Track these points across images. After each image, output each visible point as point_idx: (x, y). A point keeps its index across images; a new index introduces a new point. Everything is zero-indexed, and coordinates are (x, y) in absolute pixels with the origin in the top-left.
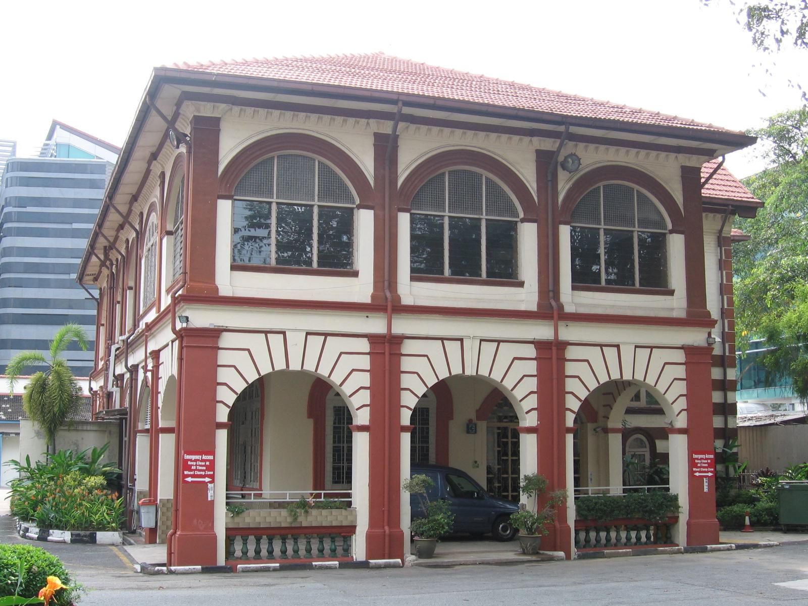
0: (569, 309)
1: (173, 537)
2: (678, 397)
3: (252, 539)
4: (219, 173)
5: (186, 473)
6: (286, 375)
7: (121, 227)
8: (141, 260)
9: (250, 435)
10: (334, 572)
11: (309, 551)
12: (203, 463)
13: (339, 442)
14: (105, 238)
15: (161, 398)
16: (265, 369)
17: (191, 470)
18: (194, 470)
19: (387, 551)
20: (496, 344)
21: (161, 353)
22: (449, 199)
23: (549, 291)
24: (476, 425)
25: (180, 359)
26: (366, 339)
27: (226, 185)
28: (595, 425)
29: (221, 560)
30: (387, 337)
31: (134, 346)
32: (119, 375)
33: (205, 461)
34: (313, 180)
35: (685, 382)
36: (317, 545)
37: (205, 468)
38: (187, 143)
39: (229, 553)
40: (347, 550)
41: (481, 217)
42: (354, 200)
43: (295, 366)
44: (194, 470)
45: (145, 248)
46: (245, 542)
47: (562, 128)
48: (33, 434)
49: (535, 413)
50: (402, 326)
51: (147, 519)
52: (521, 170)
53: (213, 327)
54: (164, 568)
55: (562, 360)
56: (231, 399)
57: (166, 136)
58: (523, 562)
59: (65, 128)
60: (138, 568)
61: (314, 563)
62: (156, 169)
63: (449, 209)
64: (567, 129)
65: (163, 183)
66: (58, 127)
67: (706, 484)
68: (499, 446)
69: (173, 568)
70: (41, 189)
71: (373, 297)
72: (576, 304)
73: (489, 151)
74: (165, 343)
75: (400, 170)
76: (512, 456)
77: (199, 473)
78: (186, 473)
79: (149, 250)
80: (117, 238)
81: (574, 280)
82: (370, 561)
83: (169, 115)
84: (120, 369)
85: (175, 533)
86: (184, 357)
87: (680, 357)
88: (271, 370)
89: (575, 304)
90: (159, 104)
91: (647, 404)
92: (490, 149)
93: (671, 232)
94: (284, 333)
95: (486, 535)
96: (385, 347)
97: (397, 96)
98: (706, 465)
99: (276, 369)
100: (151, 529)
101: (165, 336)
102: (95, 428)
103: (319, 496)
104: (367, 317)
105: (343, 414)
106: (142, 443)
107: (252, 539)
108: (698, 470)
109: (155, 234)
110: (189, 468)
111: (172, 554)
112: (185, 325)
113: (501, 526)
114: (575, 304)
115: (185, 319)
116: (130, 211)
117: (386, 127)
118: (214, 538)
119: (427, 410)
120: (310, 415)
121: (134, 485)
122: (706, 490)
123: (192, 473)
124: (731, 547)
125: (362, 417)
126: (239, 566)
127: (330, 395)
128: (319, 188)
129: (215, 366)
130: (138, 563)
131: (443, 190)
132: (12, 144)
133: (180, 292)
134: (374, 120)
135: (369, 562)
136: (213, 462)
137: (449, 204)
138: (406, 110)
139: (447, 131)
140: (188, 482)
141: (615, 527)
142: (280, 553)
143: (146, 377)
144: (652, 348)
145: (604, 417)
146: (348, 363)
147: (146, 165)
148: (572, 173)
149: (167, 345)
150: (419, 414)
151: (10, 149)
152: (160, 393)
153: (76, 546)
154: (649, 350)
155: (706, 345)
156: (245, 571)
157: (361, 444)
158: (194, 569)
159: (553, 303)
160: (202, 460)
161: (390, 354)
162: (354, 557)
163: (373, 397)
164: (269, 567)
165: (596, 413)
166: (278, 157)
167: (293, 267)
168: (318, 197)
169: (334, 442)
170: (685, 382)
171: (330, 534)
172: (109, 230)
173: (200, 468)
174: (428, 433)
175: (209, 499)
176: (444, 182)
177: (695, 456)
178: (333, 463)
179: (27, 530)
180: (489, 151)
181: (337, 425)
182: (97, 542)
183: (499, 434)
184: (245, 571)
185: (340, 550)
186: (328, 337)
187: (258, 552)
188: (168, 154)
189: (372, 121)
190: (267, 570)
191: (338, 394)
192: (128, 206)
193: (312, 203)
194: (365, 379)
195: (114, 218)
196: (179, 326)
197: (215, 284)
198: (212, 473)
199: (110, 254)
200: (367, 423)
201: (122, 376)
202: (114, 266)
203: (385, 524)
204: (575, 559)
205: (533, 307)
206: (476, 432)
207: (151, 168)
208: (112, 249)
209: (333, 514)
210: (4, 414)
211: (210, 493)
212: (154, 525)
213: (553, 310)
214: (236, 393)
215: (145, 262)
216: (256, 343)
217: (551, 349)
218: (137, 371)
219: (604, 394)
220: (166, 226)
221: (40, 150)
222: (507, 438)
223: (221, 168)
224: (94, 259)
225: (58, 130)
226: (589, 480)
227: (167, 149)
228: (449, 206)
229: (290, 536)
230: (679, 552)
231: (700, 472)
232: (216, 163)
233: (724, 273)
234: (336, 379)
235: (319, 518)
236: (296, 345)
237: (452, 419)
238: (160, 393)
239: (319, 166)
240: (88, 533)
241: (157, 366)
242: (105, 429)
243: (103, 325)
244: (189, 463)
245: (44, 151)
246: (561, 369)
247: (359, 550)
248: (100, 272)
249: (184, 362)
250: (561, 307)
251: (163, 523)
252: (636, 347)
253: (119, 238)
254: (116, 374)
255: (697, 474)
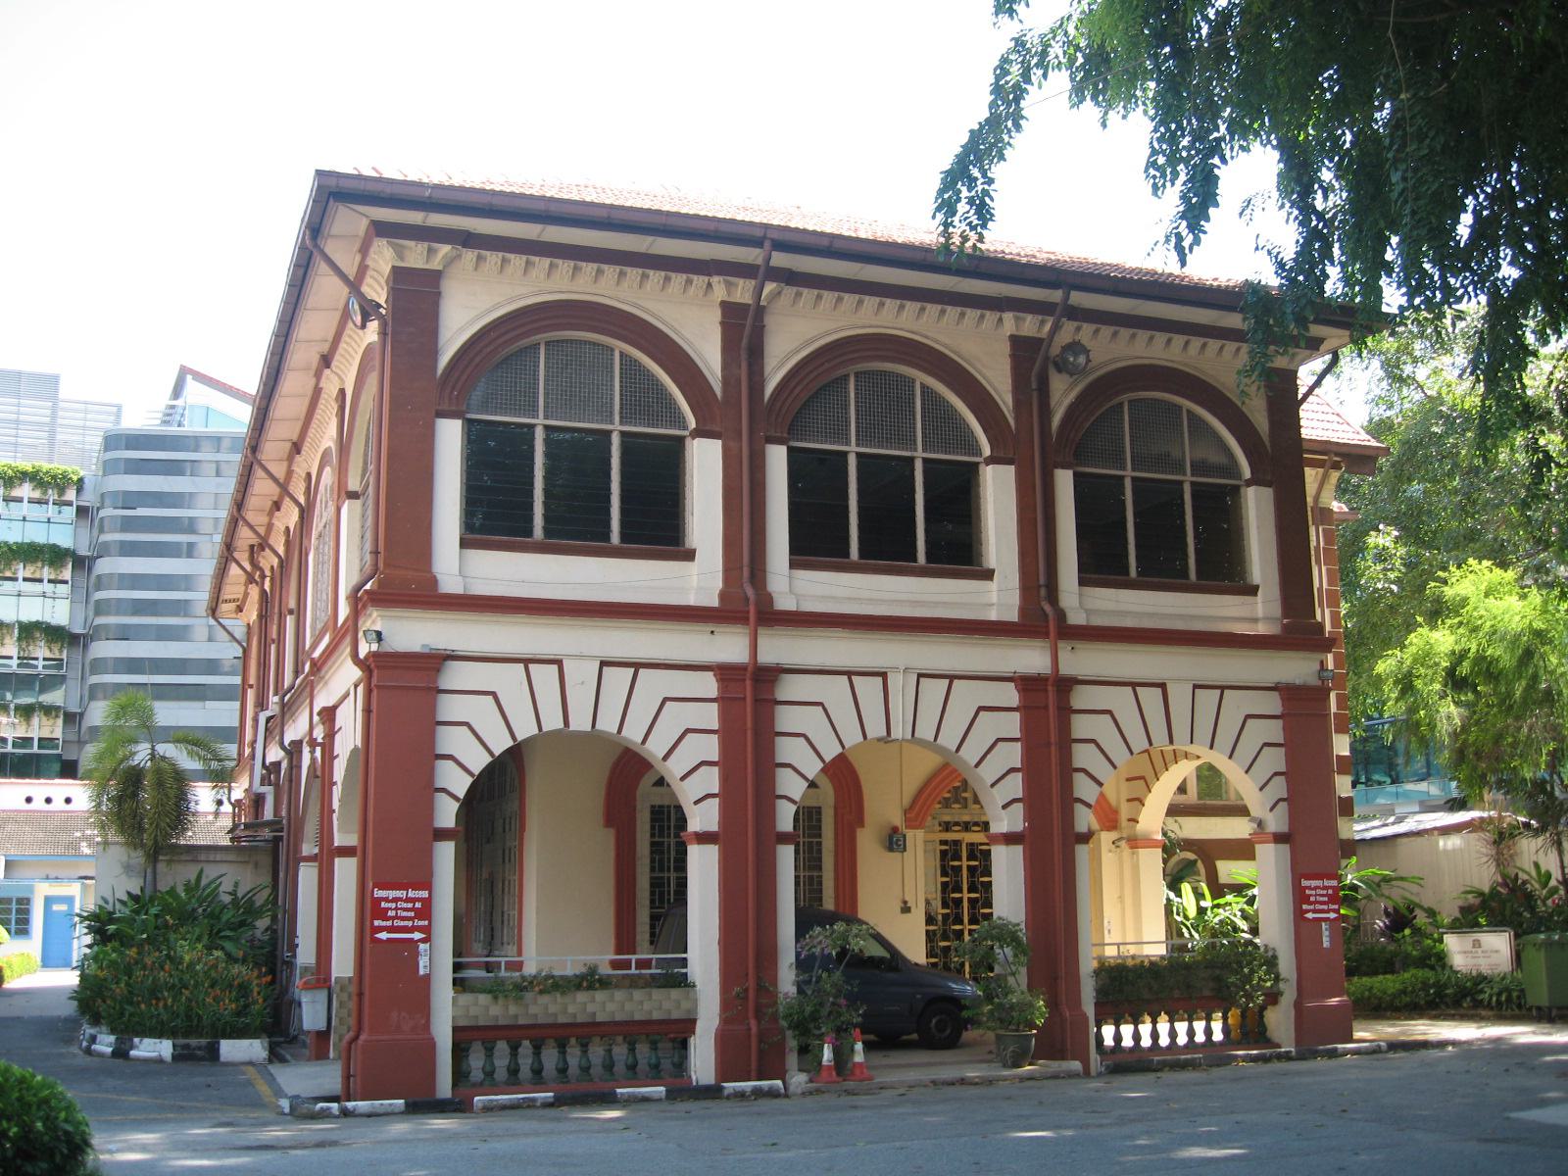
0: (1076, 618)
1: (353, 1046)
2: (1270, 779)
3: (502, 1047)
4: (440, 371)
5: (377, 923)
6: (564, 738)
7: (277, 506)
8: (307, 555)
9: (501, 860)
10: (653, 1107)
11: (609, 1066)
12: (410, 905)
13: (662, 870)
14: (251, 527)
15: (337, 792)
16: (526, 729)
17: (387, 919)
18: (393, 918)
19: (754, 1065)
20: (946, 682)
21: (339, 712)
22: (857, 423)
23: (1040, 586)
24: (904, 836)
25: (367, 711)
26: (711, 673)
27: (452, 392)
28: (1113, 835)
29: (444, 1087)
30: (749, 669)
31: (293, 709)
32: (272, 764)
33: (413, 900)
34: (611, 399)
35: (1282, 750)
36: (530, 1061)
37: (413, 914)
38: (380, 317)
39: (459, 1075)
40: (681, 1065)
41: (915, 454)
42: (684, 422)
43: (580, 722)
44: (393, 918)
45: (314, 534)
46: (489, 1052)
47: (1056, 296)
48: (119, 870)
49: (1019, 808)
50: (776, 648)
51: (312, 1013)
52: (984, 371)
53: (427, 651)
54: (335, 1105)
55: (1066, 712)
56: (461, 784)
57: (346, 315)
60: (285, 1104)
61: (619, 1090)
62: (330, 386)
63: (857, 440)
64: (1067, 297)
65: (342, 408)
66: (189, 377)
67: (1326, 934)
68: (944, 873)
69: (350, 1105)
70: (161, 478)
71: (723, 596)
72: (1089, 612)
73: (927, 337)
74: (343, 692)
75: (768, 369)
76: (969, 892)
77: (402, 923)
78: (377, 923)
79: (320, 536)
80: (270, 527)
81: (1082, 568)
82: (725, 1084)
83: (351, 272)
84: (275, 754)
85: (356, 1038)
86: (374, 707)
87: (1272, 704)
88: (536, 731)
89: (1086, 611)
90: (331, 248)
92: (929, 334)
93: (1249, 483)
94: (559, 663)
95: (905, 1037)
96: (745, 688)
97: (763, 231)
98: (1326, 899)
99: (545, 729)
100: (319, 1034)
101: (344, 676)
102: (231, 857)
103: (627, 965)
104: (712, 632)
105: (669, 819)
106: (307, 877)
107: (502, 1047)
108: (1312, 907)
109: (330, 503)
110: (382, 914)
111: (352, 1079)
112: (374, 647)
113: (934, 1021)
114: (1086, 611)
115: (374, 636)
116: (290, 473)
117: (742, 291)
118: (431, 1046)
119: (819, 810)
120: (610, 820)
121: (294, 956)
122: (1326, 943)
123: (389, 923)
124: (1379, 1046)
125: (703, 817)
126: (476, 1098)
127: (647, 781)
128: (621, 399)
129: (433, 724)
130: (286, 1096)
131: (846, 407)
132: (115, 409)
133: (368, 587)
134: (721, 278)
135: (723, 1088)
136: (427, 903)
137: (857, 431)
138: (780, 259)
139: (850, 299)
140: (380, 940)
141: (1131, 1015)
142: (555, 1072)
143: (313, 760)
144: (1222, 688)
145: (1130, 820)
146: (676, 718)
147: (313, 381)
148: (1075, 377)
149: (346, 695)
150: (808, 817)
152: (335, 783)
153: (182, 1066)
154: (1218, 692)
155: (1317, 683)
156: (488, 1109)
157: (703, 868)
158: (391, 1105)
159: (1047, 608)
160: (408, 900)
161: (756, 701)
162: (694, 1078)
163: (724, 779)
164: (534, 1100)
165: (1116, 812)
166: (547, 344)
167: (568, 436)
168: (621, 417)
169: (653, 869)
170: (1282, 750)
171: (647, 1035)
172: (255, 515)
173: (405, 914)
174: (820, 851)
175: (422, 972)
176: (847, 393)
177: (1305, 883)
178: (651, 908)
179: (93, 1039)
180: (927, 337)
181: (657, 839)
182: (222, 1059)
183: (944, 853)
184: (488, 1109)
185: (666, 1064)
186: (641, 670)
187: (513, 1071)
188: (349, 353)
189: (715, 279)
190: (530, 1104)
191: (661, 782)
192: (285, 464)
193: (609, 427)
194: (710, 748)
195: (263, 489)
196: (364, 650)
197: (430, 572)
198: (426, 923)
199: (260, 559)
200: (714, 827)
201: (277, 764)
202: (268, 580)
203: (751, 1014)
204: (1100, 1075)
205: (1013, 616)
206: (905, 850)
207: (321, 385)
208: (263, 550)
209: (654, 997)
210: (89, 846)
211: (423, 961)
212: (325, 1024)
213: (1047, 622)
214: (470, 774)
215: (314, 560)
216: (508, 680)
217: (1046, 691)
218: (300, 752)
219: (1128, 780)
220: (346, 483)
221: (160, 415)
222: (960, 859)
223: (444, 360)
224: (234, 570)
225: (193, 389)
226: (1106, 932)
227: (347, 343)
228: (857, 435)
229: (573, 1041)
230: (1280, 1057)
231: (1315, 911)
232: (434, 353)
233: (1324, 568)
234: (656, 748)
235: (628, 1007)
236: (583, 683)
237: (863, 826)
238: (335, 783)
239: (621, 360)
240: (203, 1041)
241: (331, 735)
242: (247, 859)
243: (251, 686)
244: (383, 905)
245: (168, 418)
246: (1065, 727)
247: (702, 1062)
248: (246, 595)
249: (374, 716)
250: (1061, 615)
251: (341, 1021)
252: (1195, 687)
253: (275, 528)
254: (268, 761)
255: (1310, 915)
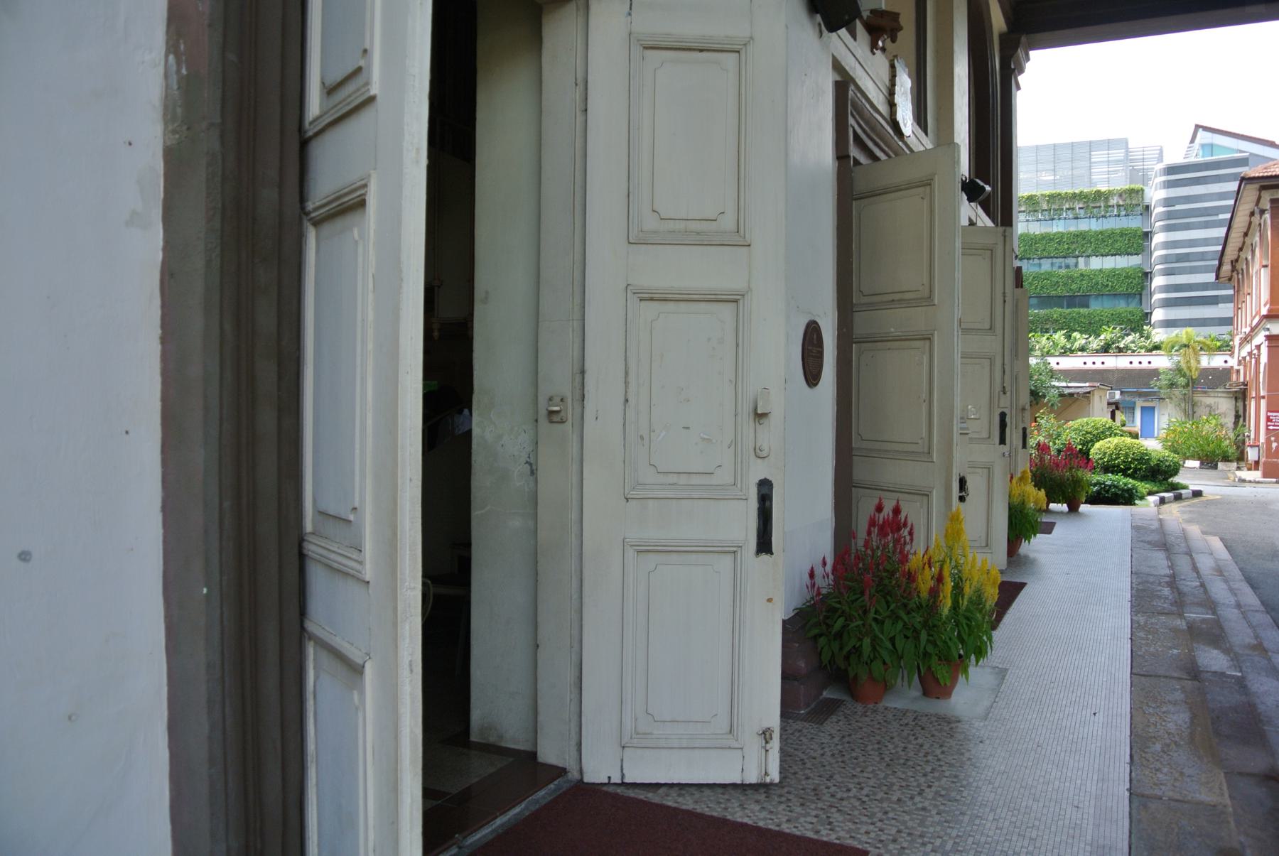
58: (1265, 483)
59: (1206, 129)
91: (1258, 470)
101: (1260, 338)
110: (1271, 421)
151: (1158, 152)
